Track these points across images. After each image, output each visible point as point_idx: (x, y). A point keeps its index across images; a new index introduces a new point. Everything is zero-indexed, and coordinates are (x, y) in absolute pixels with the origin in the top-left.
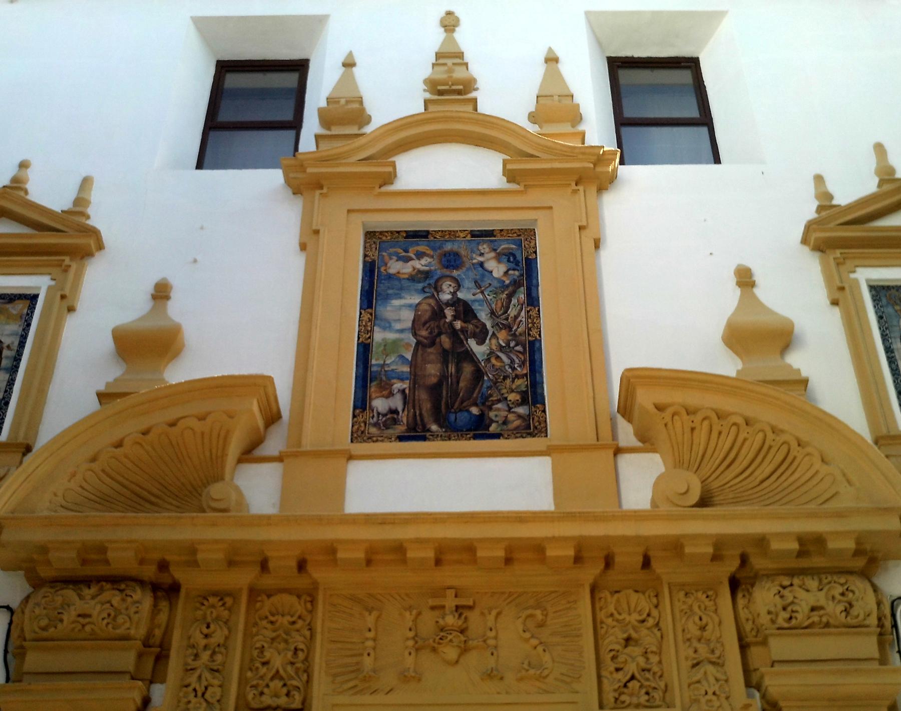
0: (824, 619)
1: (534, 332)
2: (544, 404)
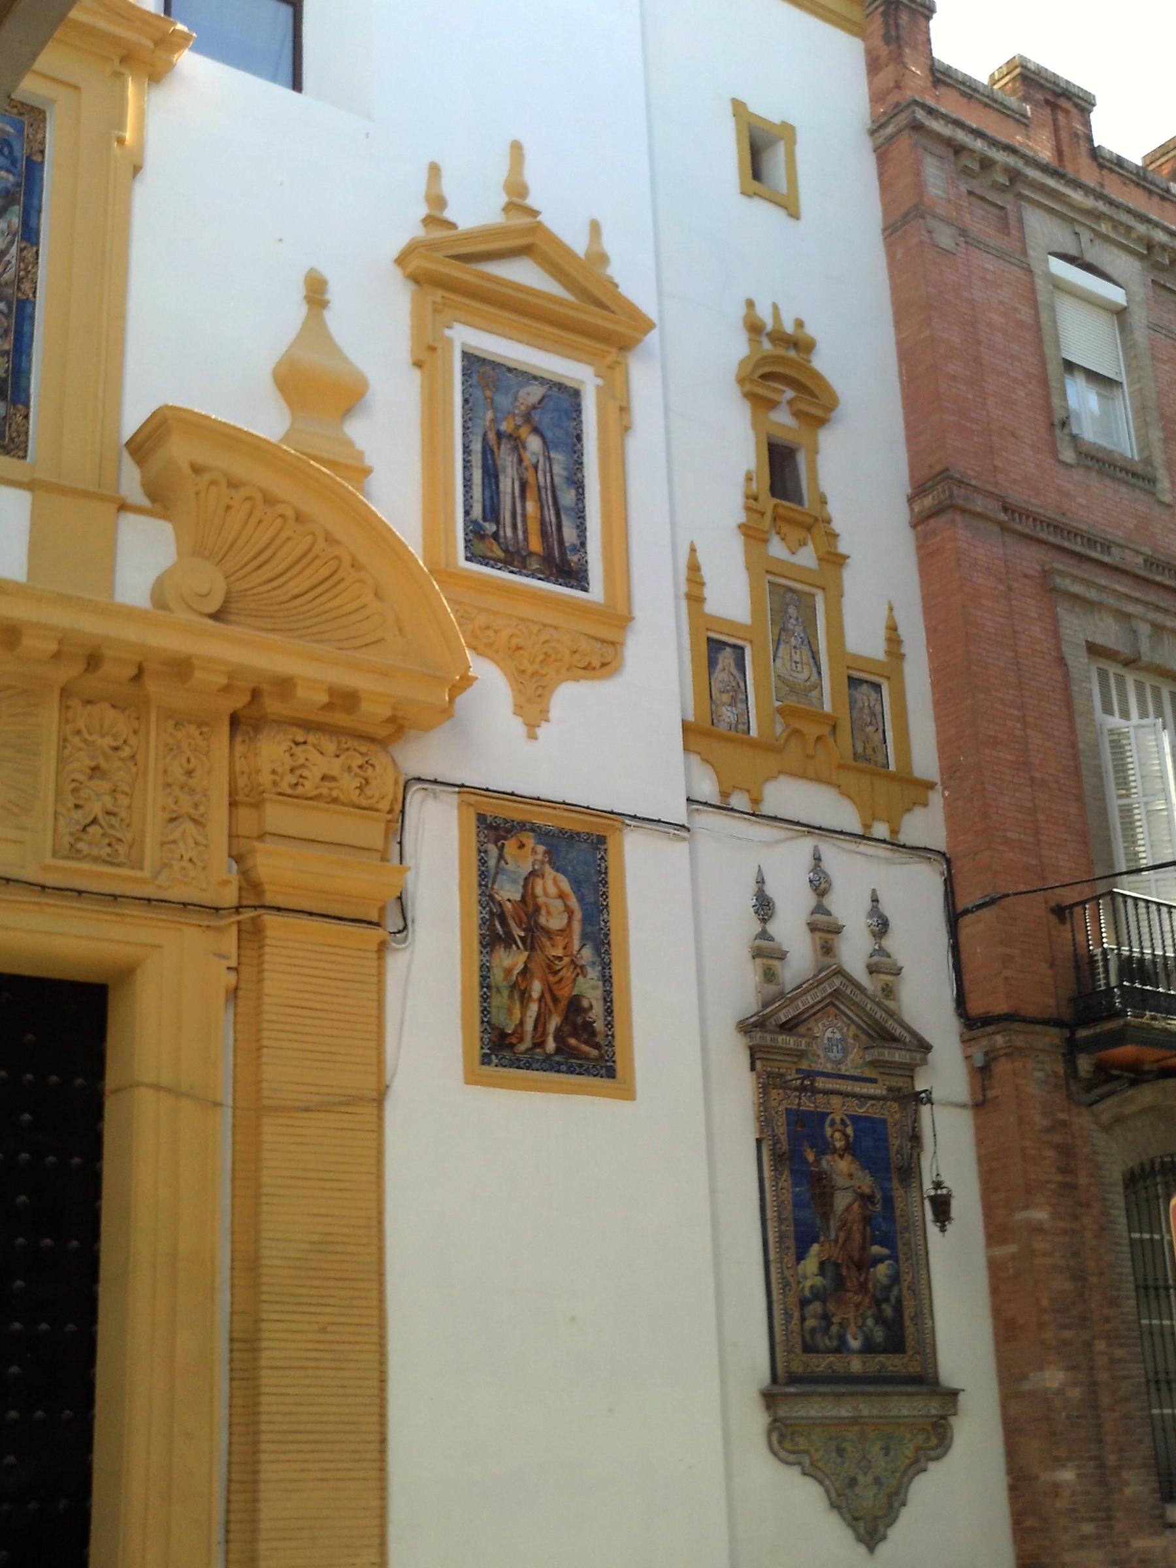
1: (26, 286)
2: (27, 406)
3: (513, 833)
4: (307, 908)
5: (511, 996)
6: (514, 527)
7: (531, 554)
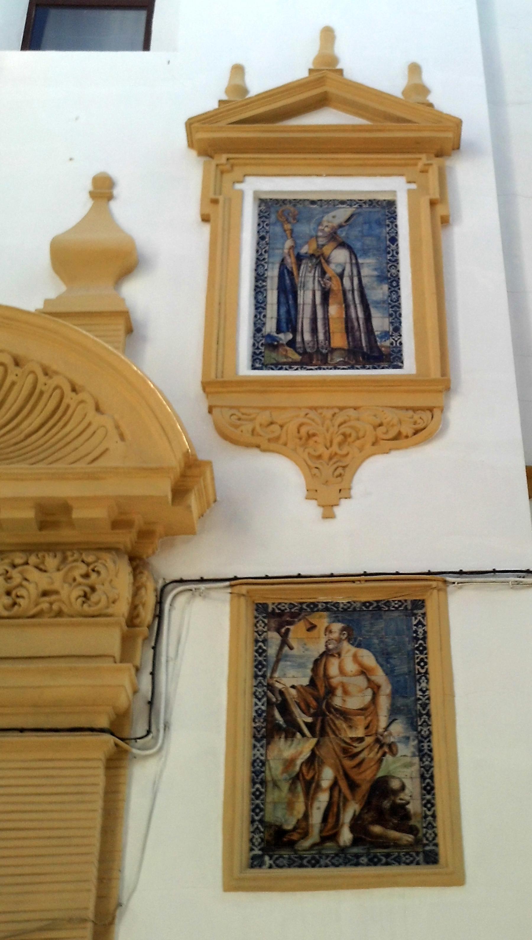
0: (55, 607)
3: (300, 617)
4: (20, 726)
5: (292, 790)
6: (314, 331)
7: (333, 350)
